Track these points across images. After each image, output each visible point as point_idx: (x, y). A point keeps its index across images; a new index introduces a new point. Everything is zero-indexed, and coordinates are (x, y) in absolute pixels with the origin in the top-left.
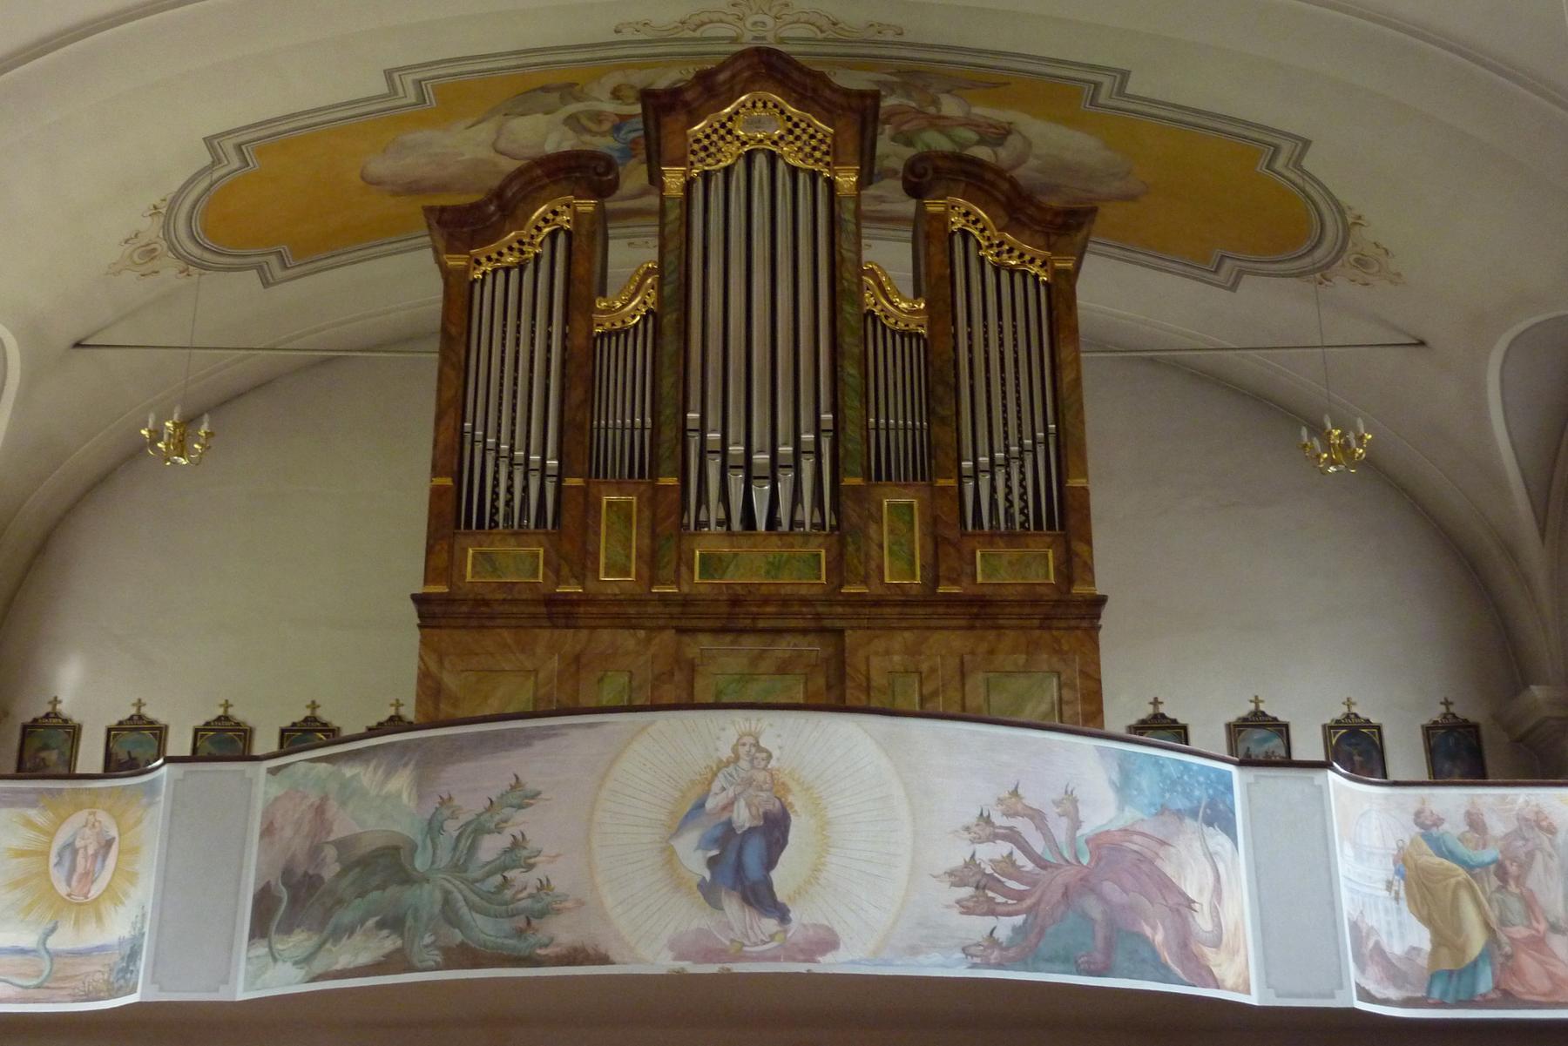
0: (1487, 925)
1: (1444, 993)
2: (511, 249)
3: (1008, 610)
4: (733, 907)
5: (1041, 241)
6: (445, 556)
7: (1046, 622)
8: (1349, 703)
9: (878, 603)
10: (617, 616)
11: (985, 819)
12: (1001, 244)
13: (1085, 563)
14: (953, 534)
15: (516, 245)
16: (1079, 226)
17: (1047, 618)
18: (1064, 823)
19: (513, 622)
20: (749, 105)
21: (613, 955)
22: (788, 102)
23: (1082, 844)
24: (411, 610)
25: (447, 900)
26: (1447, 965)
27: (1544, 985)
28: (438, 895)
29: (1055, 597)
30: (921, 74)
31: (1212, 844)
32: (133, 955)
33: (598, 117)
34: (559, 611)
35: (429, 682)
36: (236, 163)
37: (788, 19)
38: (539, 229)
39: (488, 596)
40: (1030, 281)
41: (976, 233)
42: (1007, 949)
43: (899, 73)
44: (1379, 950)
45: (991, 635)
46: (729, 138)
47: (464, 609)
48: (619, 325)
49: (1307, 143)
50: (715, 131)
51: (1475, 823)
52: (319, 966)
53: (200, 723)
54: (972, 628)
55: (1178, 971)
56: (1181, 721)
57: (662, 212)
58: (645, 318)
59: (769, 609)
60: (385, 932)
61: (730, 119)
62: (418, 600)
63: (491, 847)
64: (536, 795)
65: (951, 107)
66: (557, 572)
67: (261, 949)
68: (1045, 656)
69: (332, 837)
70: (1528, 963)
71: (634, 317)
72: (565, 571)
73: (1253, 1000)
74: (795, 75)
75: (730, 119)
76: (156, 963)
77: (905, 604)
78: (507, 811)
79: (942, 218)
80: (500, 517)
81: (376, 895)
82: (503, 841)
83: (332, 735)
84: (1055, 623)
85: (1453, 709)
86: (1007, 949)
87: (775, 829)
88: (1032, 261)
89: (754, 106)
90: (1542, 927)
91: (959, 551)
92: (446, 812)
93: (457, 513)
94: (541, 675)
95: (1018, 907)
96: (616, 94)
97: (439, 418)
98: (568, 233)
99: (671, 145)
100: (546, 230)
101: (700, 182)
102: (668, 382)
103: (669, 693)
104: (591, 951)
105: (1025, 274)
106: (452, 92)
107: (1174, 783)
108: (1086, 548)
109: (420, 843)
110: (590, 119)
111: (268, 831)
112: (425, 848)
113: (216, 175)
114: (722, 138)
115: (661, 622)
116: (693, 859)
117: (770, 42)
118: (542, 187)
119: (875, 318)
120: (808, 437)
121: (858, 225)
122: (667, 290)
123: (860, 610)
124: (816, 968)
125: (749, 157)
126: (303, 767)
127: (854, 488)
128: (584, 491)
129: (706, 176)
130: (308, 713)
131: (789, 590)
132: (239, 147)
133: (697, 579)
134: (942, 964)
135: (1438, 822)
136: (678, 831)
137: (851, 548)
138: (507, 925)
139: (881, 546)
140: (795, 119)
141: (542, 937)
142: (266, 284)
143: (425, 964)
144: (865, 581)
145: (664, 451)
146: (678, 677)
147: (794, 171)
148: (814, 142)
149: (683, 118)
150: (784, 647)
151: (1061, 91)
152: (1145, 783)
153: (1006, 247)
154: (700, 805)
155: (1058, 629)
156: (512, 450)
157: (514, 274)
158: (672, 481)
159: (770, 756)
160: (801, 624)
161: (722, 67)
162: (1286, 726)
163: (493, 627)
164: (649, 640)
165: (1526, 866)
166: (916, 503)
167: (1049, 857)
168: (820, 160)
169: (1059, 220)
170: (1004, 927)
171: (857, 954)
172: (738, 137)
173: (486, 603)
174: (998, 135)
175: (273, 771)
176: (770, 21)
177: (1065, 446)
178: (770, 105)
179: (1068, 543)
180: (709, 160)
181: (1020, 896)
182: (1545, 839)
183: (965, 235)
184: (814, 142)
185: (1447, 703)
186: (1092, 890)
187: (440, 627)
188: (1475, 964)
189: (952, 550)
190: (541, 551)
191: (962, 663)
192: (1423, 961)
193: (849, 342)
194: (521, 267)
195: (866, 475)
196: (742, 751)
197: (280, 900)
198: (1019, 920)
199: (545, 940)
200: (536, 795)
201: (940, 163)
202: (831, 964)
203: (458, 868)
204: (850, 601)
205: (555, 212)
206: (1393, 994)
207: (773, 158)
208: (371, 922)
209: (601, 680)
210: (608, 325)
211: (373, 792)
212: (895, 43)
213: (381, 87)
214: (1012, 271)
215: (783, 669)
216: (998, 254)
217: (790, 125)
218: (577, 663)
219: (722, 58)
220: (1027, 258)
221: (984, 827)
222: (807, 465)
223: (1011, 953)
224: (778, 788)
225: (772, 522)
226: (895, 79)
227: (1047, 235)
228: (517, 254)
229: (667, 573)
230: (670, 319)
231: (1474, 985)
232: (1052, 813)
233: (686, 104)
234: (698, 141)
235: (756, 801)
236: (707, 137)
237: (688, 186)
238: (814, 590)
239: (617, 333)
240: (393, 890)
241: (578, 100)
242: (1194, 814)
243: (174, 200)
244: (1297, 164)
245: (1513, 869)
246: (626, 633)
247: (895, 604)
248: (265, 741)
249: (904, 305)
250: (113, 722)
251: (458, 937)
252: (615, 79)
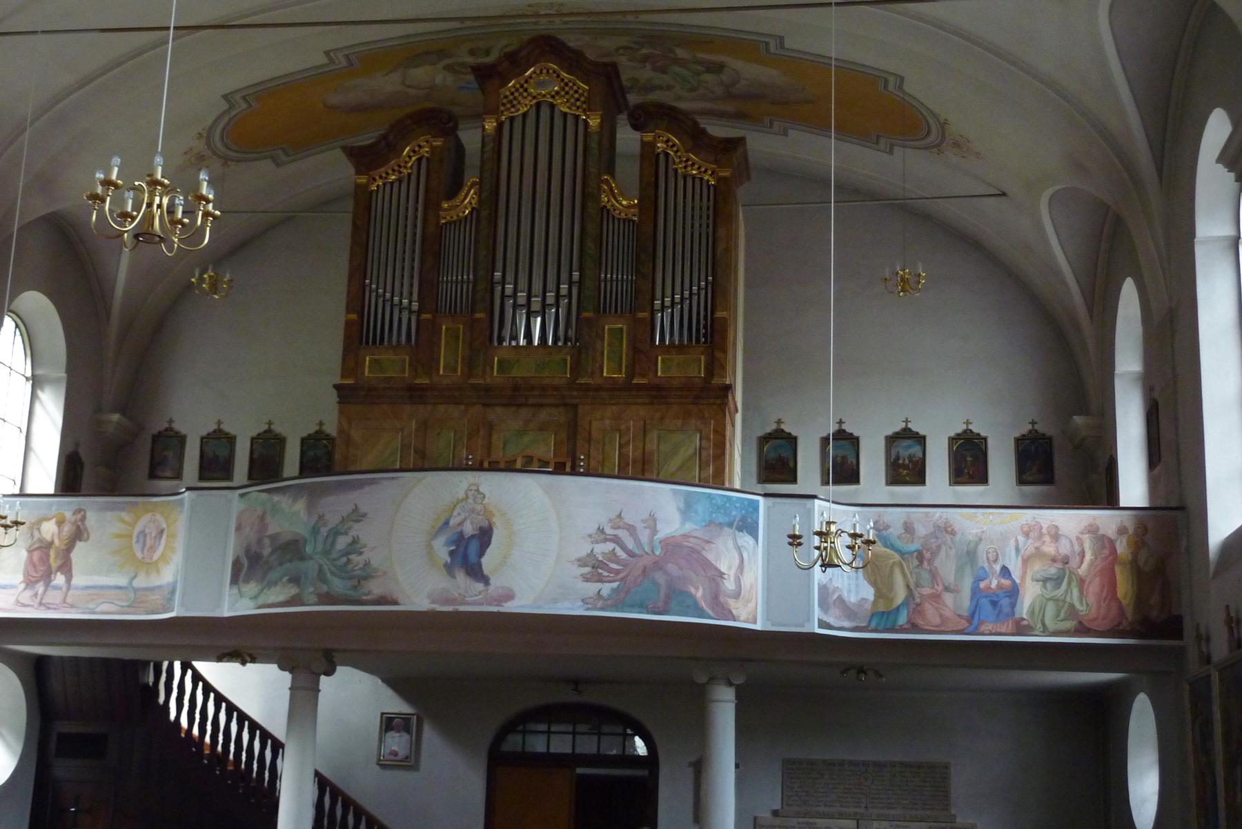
0: (908, 586)
1: (878, 624)
4: (461, 577)
8: (968, 423)
9: (598, 389)
11: (601, 531)
12: (687, 160)
18: (647, 532)
21: (400, 601)
23: (657, 543)
24: (333, 397)
25: (321, 570)
26: (882, 609)
27: (937, 621)
28: (316, 567)
31: (740, 542)
32: (173, 592)
33: (463, 64)
34: (415, 394)
36: (244, 106)
38: (410, 157)
44: (841, 600)
48: (455, 218)
51: (908, 528)
52: (261, 601)
53: (254, 434)
54: (652, 404)
55: (710, 612)
56: (855, 434)
58: (471, 213)
59: (537, 393)
63: (342, 542)
64: (364, 515)
67: (235, 591)
69: (269, 533)
70: (929, 610)
73: (758, 627)
76: (184, 594)
81: (288, 565)
82: (348, 539)
85: (1036, 427)
87: (485, 536)
88: (706, 171)
90: (940, 588)
93: (360, 335)
96: (472, 53)
107: (719, 508)
111: (239, 528)
113: (233, 113)
114: (521, 94)
116: (442, 551)
119: (608, 211)
122: (484, 195)
124: (502, 610)
129: (512, 119)
131: (547, 381)
134: (572, 608)
135: (887, 527)
136: (435, 535)
137: (584, 356)
141: (365, 590)
144: (592, 375)
147: (565, 115)
150: (543, 415)
152: (700, 508)
154: (447, 523)
156: (392, 296)
162: (924, 438)
165: (935, 554)
167: (637, 551)
170: (606, 589)
171: (522, 604)
175: (242, 496)
181: (617, 572)
182: (948, 537)
183: (667, 154)
185: (1033, 423)
188: (898, 609)
190: (407, 358)
192: (868, 606)
195: (597, 310)
196: (470, 493)
198: (615, 585)
200: (364, 515)
202: (510, 607)
203: (326, 553)
206: (846, 624)
208: (285, 579)
213: (323, 60)
214: (694, 177)
216: (685, 167)
218: (424, 426)
221: (601, 535)
223: (609, 602)
224: (488, 514)
230: (484, 213)
231: (896, 620)
232: (640, 526)
234: (506, 97)
237: (500, 126)
242: (730, 525)
245: (927, 555)
249: (624, 203)
250: (204, 433)
251: (325, 588)
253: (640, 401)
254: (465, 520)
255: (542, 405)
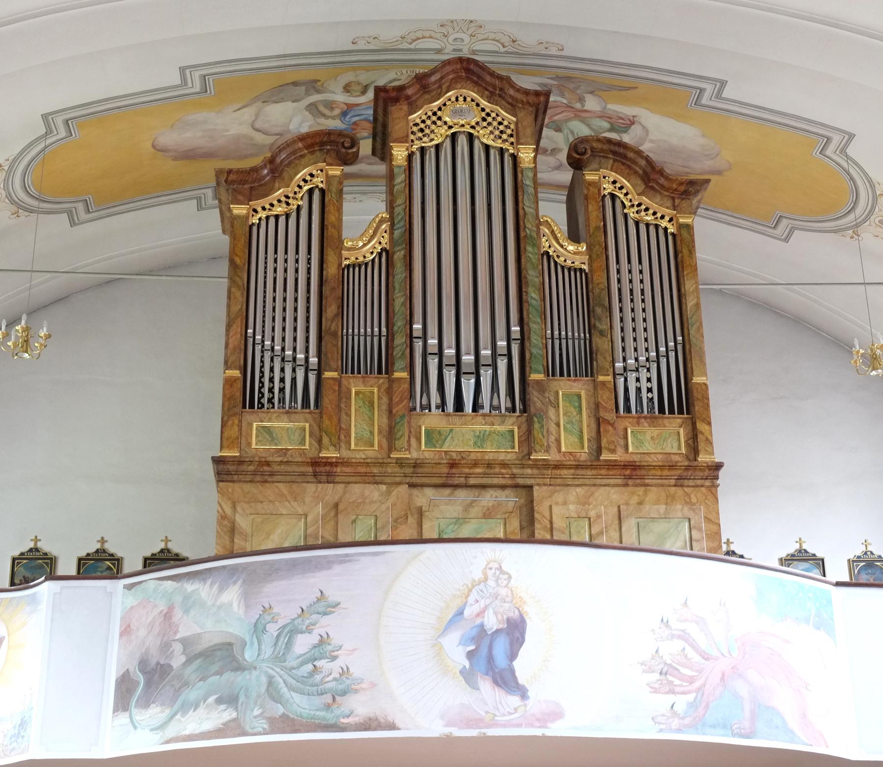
2: (279, 201)
3: (652, 472)
4: (486, 685)
5: (669, 203)
6: (236, 428)
7: (680, 481)
9: (557, 467)
10: (366, 474)
12: (639, 205)
13: (707, 439)
14: (610, 416)
15: (283, 199)
16: (698, 192)
17: (680, 478)
19: (288, 478)
20: (453, 99)
21: (398, 723)
22: (482, 97)
25: (271, 683)
28: (264, 680)
29: (686, 463)
30: (580, 79)
33: (330, 105)
34: (322, 470)
35: (226, 522)
36: (63, 133)
37: (480, 37)
39: (270, 459)
40: (661, 232)
41: (622, 196)
42: (683, 718)
43: (558, 78)
45: (641, 490)
46: (439, 123)
47: (251, 468)
48: (361, 259)
49: (851, 136)
50: (429, 117)
52: (171, 731)
54: (626, 485)
57: (391, 176)
59: (478, 470)
60: (223, 707)
61: (440, 109)
62: (218, 461)
63: (303, 644)
65: (592, 104)
66: (320, 442)
68: (679, 507)
69: (178, 636)
71: (372, 253)
72: (326, 440)
74: (488, 78)
75: (440, 109)
77: (577, 467)
78: (314, 616)
79: (597, 185)
80: (265, 401)
81: (215, 679)
82: (314, 639)
83: (179, 560)
84: (686, 482)
86: (683, 718)
87: (515, 631)
88: (662, 217)
89: (457, 99)
91: (615, 429)
92: (268, 618)
93: (246, 396)
94: (309, 518)
95: (690, 688)
96: (347, 89)
97: (229, 326)
98: (322, 191)
99: (396, 128)
100: (306, 188)
101: (418, 155)
102: (399, 300)
103: (407, 532)
104: (382, 720)
105: (657, 226)
106: (223, 84)
108: (707, 427)
109: (247, 639)
110: (325, 107)
111: (126, 631)
112: (252, 644)
113: (48, 142)
114: (434, 123)
115: (398, 479)
116: (456, 652)
117: (465, 53)
118: (302, 156)
120: (502, 344)
121: (536, 189)
122: (397, 233)
123: (545, 472)
124: (549, 733)
125: (454, 137)
126: (152, 585)
127: (538, 382)
128: (338, 381)
130: (98, 546)
131: (490, 457)
132: (66, 122)
133: (423, 447)
137: (537, 426)
138: (318, 701)
139: (558, 425)
140: (488, 110)
141: (345, 709)
142: (73, 224)
143: (255, 730)
145: (397, 352)
146: (411, 520)
147: (487, 148)
148: (501, 128)
149: (405, 107)
150: (488, 498)
151: (679, 94)
153: (643, 207)
154: (460, 613)
155: (688, 486)
156: (283, 349)
157: (282, 220)
158: (405, 375)
159: (510, 577)
160: (502, 481)
161: (433, 72)
163: (273, 482)
164: (389, 493)
166: (583, 393)
168: (506, 141)
169: (682, 188)
170: (682, 702)
172: (445, 123)
173: (268, 464)
174: (629, 123)
175: (130, 587)
176: (466, 38)
177: (687, 355)
178: (469, 99)
179: (694, 425)
180: (425, 139)
181: (691, 680)
183: (613, 197)
184: (501, 128)
186: (740, 676)
187: (233, 481)
189: (610, 428)
190: (307, 425)
191: (619, 511)
193: (532, 275)
194: (288, 216)
196: (490, 573)
197: (138, 683)
198: (691, 697)
199: (347, 712)
201: (595, 145)
202: (558, 729)
203: (279, 659)
204: (536, 465)
205: (315, 173)
207: (471, 137)
208: (212, 699)
209: (354, 521)
210: (353, 259)
211: (210, 603)
212: (557, 57)
215: (487, 515)
216: (637, 212)
217: (483, 114)
219: (436, 64)
220: (659, 215)
222: (502, 364)
223: (687, 721)
225: (476, 407)
226: (555, 83)
227: (673, 199)
228: (284, 205)
229: (402, 443)
230: (399, 255)
233: (408, 98)
234: (416, 125)
235: (501, 610)
236: (423, 122)
237: (410, 157)
238: (509, 457)
239: (354, 266)
240: (228, 676)
241: (318, 92)
243: (15, 160)
244: (843, 151)
246: (372, 487)
247: (570, 467)
248: (67, 565)
249: (571, 248)
251: (281, 710)
252: (349, 77)
253: (612, 481)
254: (486, 607)
255: (484, 487)
